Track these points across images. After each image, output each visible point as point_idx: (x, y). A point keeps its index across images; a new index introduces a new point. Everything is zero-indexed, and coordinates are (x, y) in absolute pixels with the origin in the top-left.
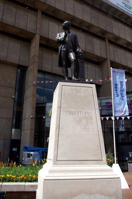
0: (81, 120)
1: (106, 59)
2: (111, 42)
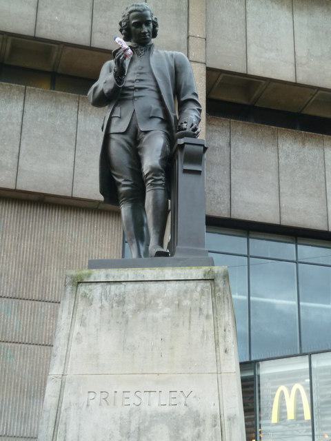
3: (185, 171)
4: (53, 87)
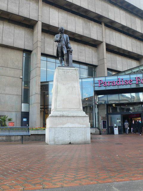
1: (102, 42)
2: (106, 25)
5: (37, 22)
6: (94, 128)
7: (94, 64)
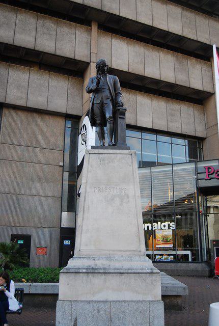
0: (113, 199)
3: (120, 118)
4: (40, 69)
5: (88, 64)
6: (199, 263)
7: (199, 135)
